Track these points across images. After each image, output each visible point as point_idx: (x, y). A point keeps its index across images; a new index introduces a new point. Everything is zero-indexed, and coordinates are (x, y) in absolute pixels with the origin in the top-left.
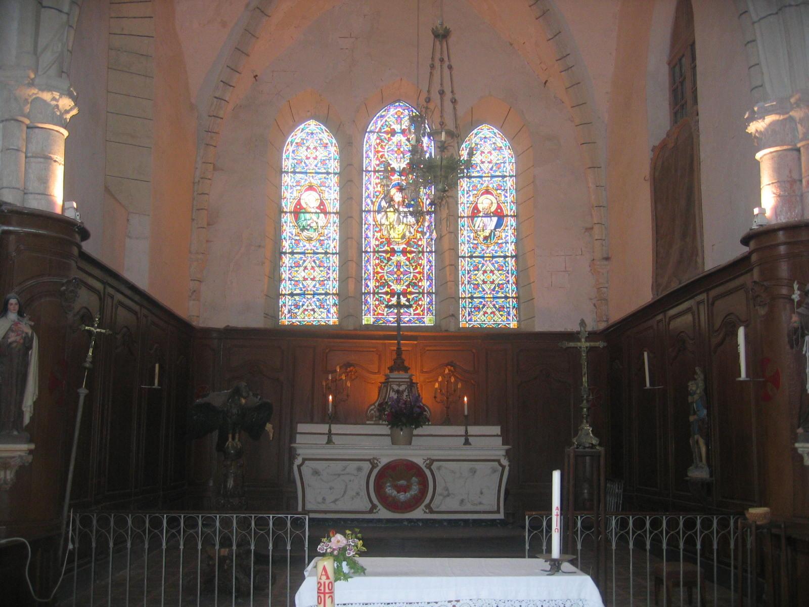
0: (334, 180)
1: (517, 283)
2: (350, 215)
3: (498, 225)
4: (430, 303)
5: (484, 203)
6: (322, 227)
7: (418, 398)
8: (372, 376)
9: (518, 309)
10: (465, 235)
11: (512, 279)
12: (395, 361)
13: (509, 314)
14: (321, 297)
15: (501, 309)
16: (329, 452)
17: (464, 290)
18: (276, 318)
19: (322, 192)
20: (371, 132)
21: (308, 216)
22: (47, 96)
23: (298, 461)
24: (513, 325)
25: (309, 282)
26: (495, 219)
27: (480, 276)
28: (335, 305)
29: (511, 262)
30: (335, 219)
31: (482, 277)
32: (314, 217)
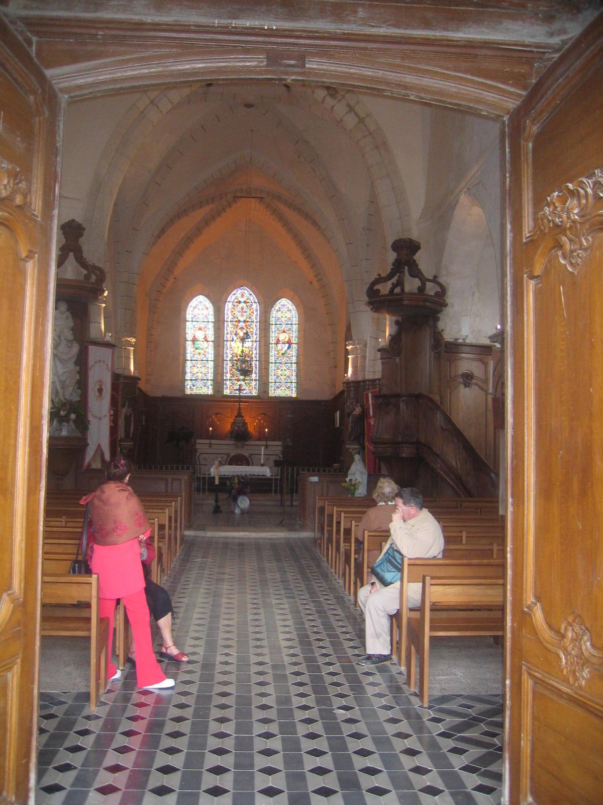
0: (211, 325)
1: (297, 376)
2: (219, 343)
3: (289, 348)
4: (256, 385)
5: (283, 337)
6: (206, 348)
7: (246, 430)
8: (228, 419)
9: (297, 388)
10: (273, 353)
11: (294, 374)
12: (238, 413)
13: (292, 390)
14: (205, 381)
15: (289, 388)
16: (210, 451)
17: (272, 379)
18: (184, 391)
19: (206, 331)
20: (229, 302)
21: (199, 342)
22: (129, 339)
23: (198, 454)
24: (294, 395)
25: (199, 374)
26: (287, 345)
27: (279, 372)
28: (211, 385)
29: (294, 366)
30: (211, 344)
31: (280, 373)
32: (202, 343)
